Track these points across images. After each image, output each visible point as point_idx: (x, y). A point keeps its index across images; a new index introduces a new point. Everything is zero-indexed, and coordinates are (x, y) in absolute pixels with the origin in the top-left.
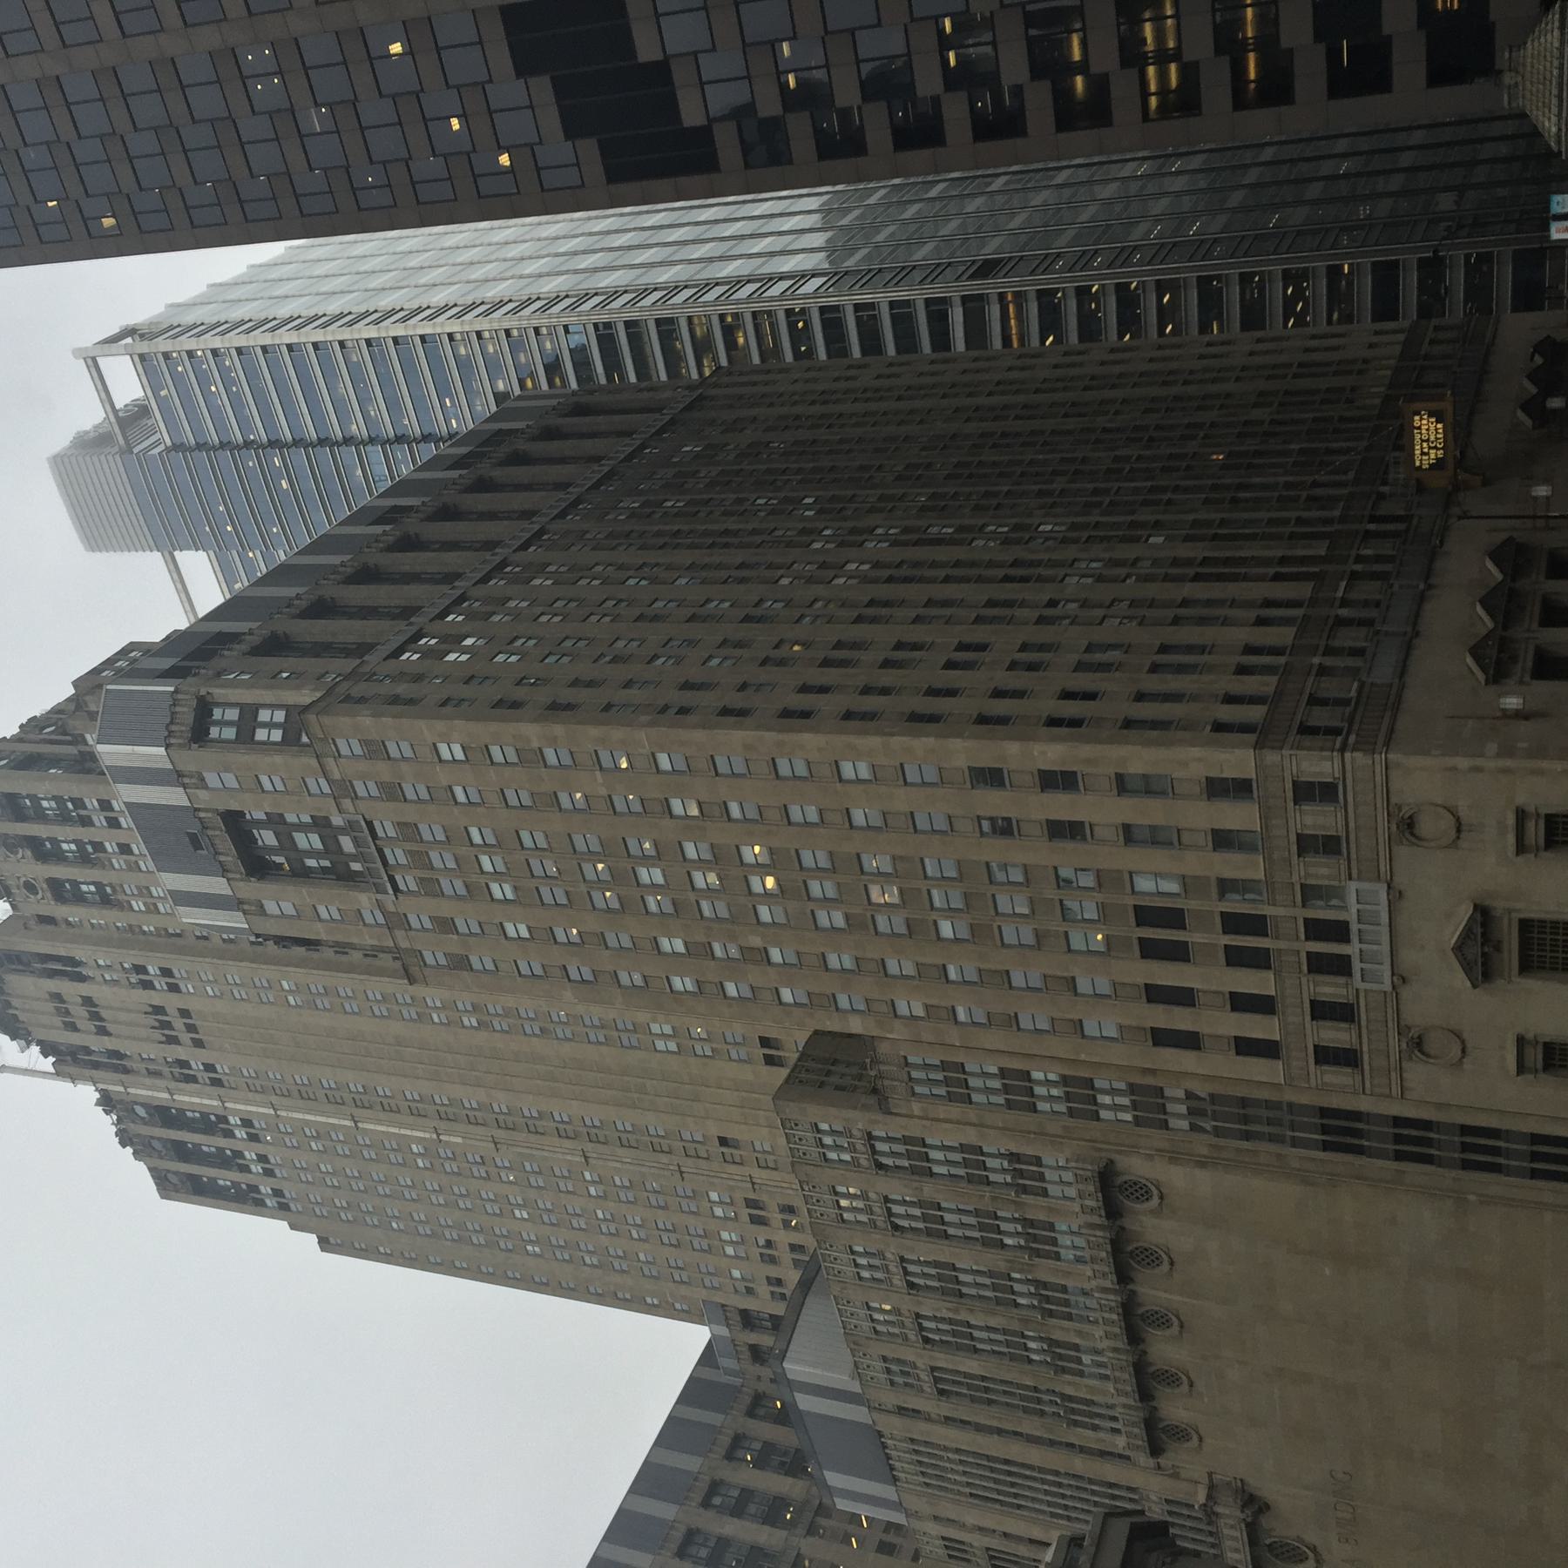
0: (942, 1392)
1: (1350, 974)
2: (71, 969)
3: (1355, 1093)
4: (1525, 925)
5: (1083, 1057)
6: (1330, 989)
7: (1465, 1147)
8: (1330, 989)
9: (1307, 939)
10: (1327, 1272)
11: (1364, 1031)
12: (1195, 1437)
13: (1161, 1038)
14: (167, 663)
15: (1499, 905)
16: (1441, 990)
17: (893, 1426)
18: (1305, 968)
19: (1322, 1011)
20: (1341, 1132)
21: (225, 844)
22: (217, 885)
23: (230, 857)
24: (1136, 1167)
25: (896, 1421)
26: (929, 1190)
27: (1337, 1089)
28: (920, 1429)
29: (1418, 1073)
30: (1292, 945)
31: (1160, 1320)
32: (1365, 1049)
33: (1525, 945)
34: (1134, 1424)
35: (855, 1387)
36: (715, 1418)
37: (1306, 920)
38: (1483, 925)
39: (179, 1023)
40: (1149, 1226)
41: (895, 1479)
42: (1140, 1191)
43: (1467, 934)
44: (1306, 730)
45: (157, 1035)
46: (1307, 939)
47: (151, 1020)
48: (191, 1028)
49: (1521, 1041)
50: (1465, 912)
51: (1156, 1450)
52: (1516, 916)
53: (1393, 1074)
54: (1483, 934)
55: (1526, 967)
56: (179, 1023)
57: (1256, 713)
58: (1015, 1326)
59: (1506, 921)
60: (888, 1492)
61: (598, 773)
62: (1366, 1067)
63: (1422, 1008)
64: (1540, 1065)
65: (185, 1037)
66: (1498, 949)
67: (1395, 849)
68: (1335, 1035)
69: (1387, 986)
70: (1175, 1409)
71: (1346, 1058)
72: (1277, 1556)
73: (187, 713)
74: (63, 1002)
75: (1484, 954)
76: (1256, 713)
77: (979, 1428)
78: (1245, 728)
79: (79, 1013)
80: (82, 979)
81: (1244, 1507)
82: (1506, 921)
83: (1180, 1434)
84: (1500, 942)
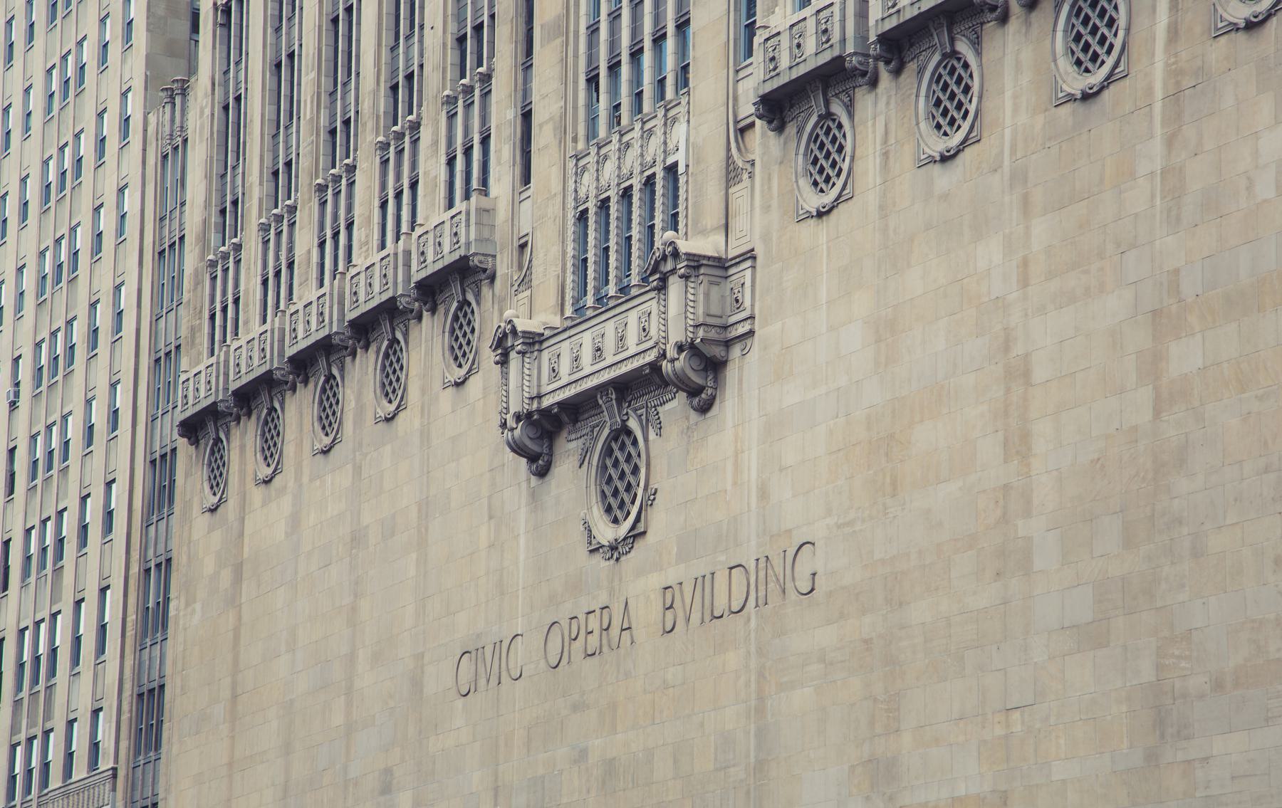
51: (777, 107)
72: (608, 451)
83: (826, 161)
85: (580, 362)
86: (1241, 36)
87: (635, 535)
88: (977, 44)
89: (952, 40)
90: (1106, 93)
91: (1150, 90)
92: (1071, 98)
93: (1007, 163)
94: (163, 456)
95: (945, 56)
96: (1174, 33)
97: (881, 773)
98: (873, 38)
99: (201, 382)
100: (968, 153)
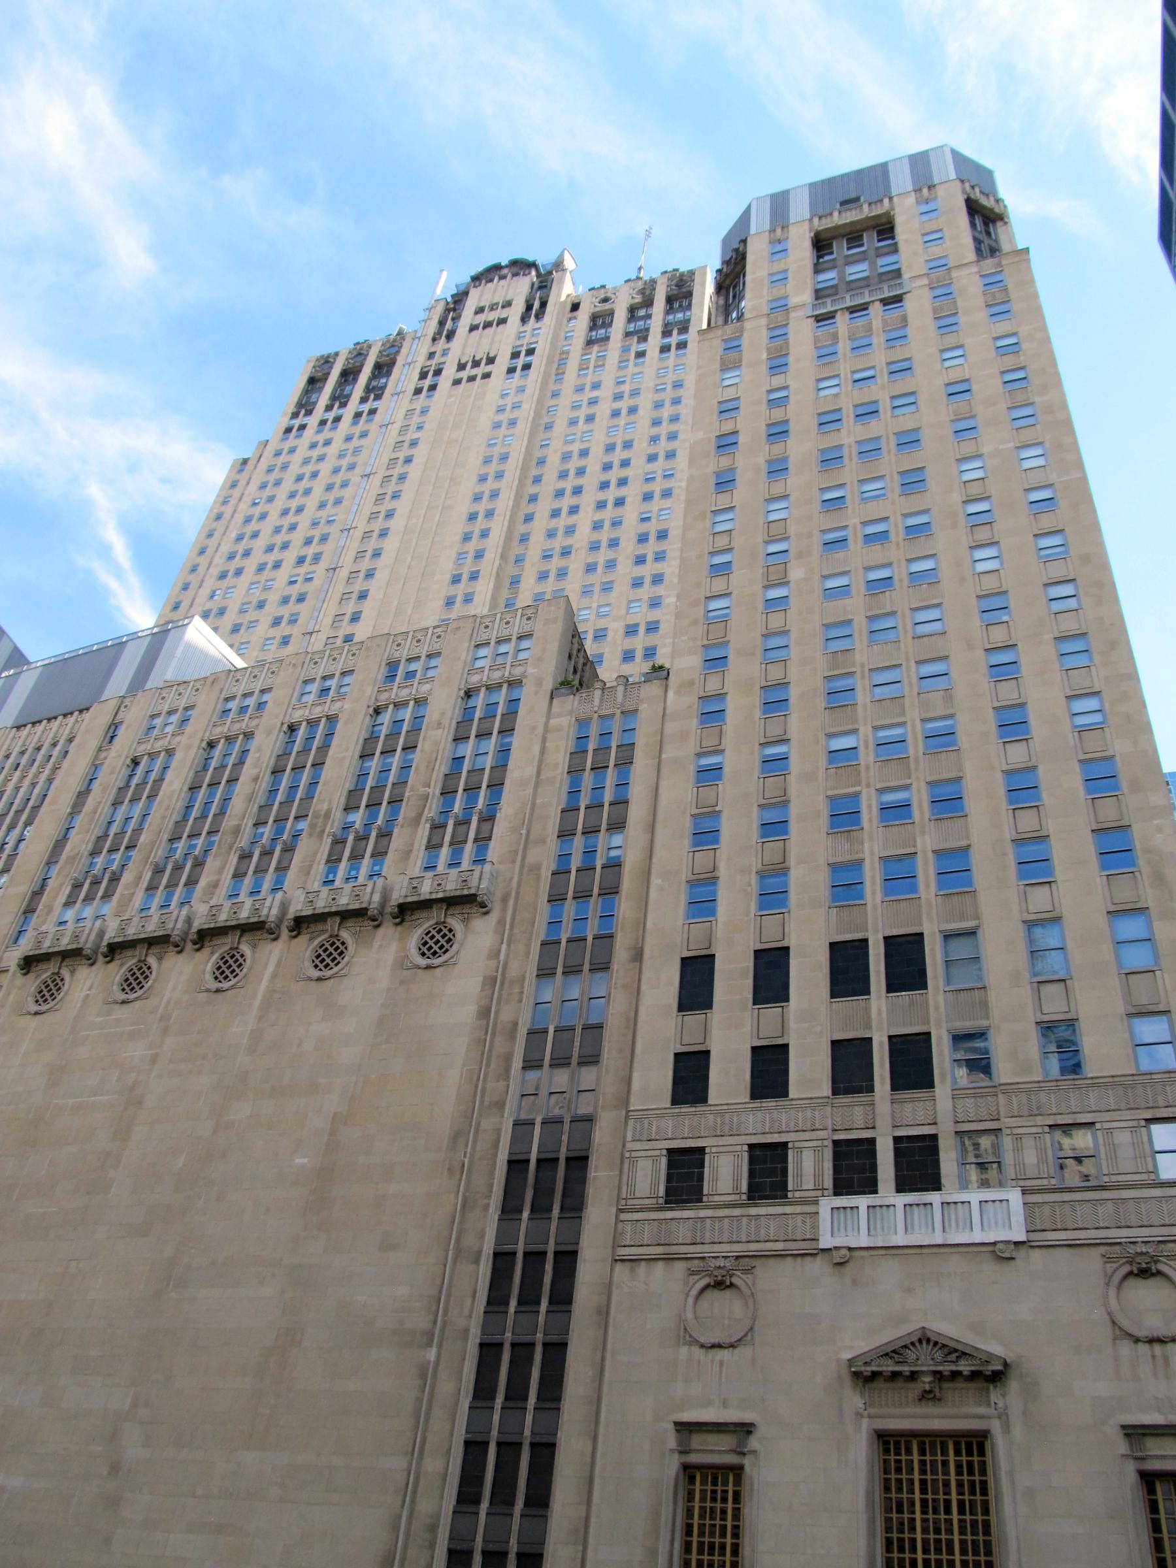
1: (837, 1193)
4: (975, 1444)
5: (655, 881)
6: (809, 1167)
7: (522, 1350)
8: (809, 1167)
9: (897, 1140)
10: (299, 1161)
11: (737, 1212)
15: (1011, 1397)
17: (98, 718)
18: (842, 1136)
24: (476, 939)
26: (486, 670)
27: (622, 1174)
30: (884, 1116)
32: (703, 1213)
33: (928, 1440)
34: (76, 937)
35: (153, 682)
37: (934, 1137)
38: (975, 1375)
40: (379, 957)
41: (18, 728)
42: (437, 946)
46: (897, 1140)
49: (745, 1429)
52: (995, 1427)
53: (660, 1250)
54: (955, 1375)
55: (888, 1442)
58: (228, 823)
59: (982, 1410)
61: (1012, 445)
62: (669, 1215)
63: (783, 1288)
64: (694, 1458)
66: (926, 1396)
67: (1096, 1253)
68: (726, 1173)
69: (826, 1242)
70: (87, 985)
75: (913, 1376)
82: (982, 1410)
83: (49, 993)
84: (936, 1400)
86: (313, 984)
88: (73, 972)
89: (60, 968)
90: (229, 993)
91: (254, 996)
92: (208, 990)
93: (161, 1010)
94: (547, 1163)
95: (139, 961)
96: (275, 976)
97: (1020, 1565)
98: (105, 943)
99: (60, 923)
100: (138, 1004)
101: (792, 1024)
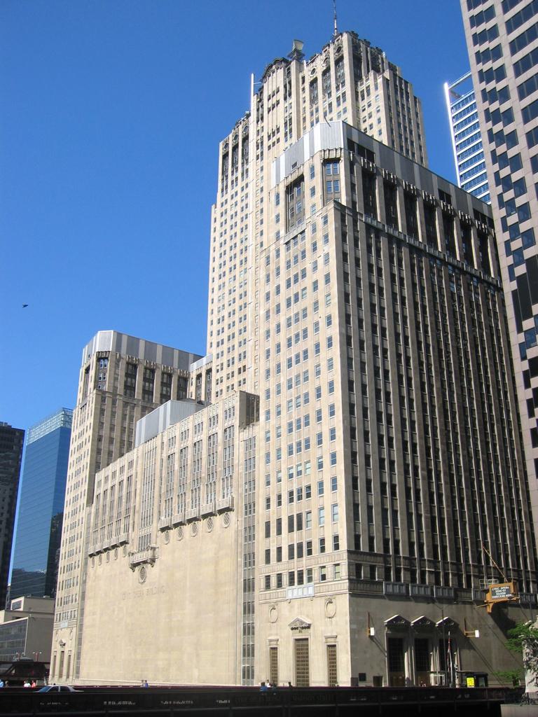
0: (195, 444)
2: (288, 95)
3: (259, 589)
6: (285, 579)
8: (285, 579)
12: (227, 526)
13: (268, 525)
14: (355, 139)
16: (289, 614)
19: (279, 577)
20: (249, 586)
21: (295, 176)
22: (283, 176)
23: (291, 179)
25: (160, 441)
27: (260, 583)
28: (159, 450)
29: (266, 608)
31: (210, 525)
36: (176, 365)
39: (274, 139)
43: (302, 622)
44: (358, 567)
45: (270, 132)
47: (275, 128)
48: (274, 144)
50: (308, 621)
56: (274, 139)
57: (364, 547)
60: (143, 441)
63: (284, 607)
65: (270, 143)
67: (323, 598)
68: (274, 581)
71: (268, 586)
73: (333, 155)
74: (273, 96)
76: (364, 547)
77: (161, 470)
78: (357, 545)
79: (274, 100)
80: (285, 99)
81: (151, 559)
85: (139, 557)
87: (144, 582)
101: (283, 541)
